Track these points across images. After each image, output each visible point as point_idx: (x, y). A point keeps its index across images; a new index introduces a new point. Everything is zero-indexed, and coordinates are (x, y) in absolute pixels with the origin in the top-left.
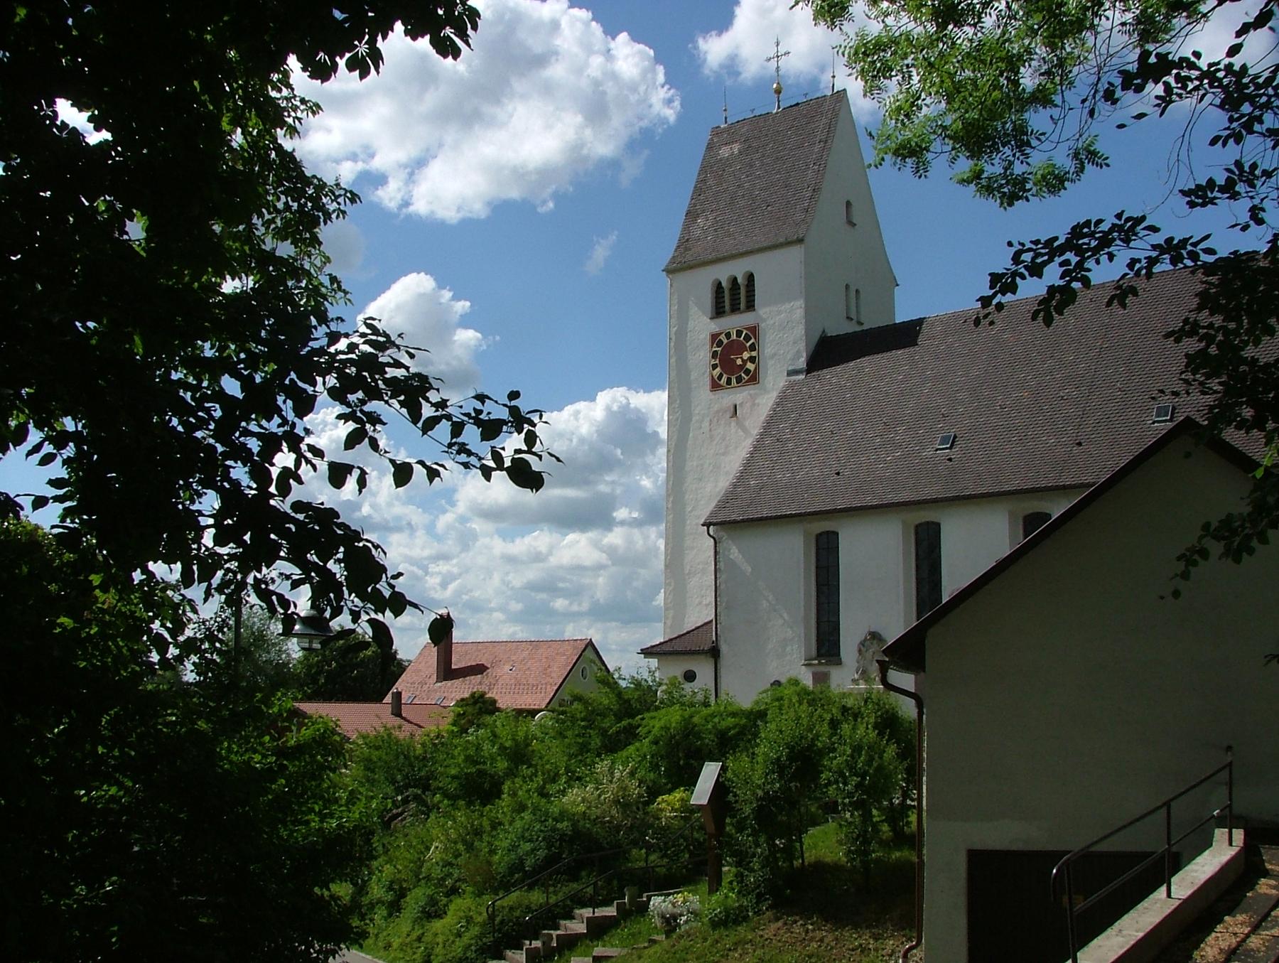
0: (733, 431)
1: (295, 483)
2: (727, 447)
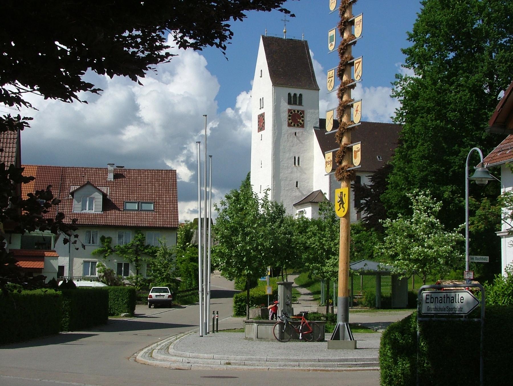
0: (295, 140)
1: (74, 98)
2: (293, 144)
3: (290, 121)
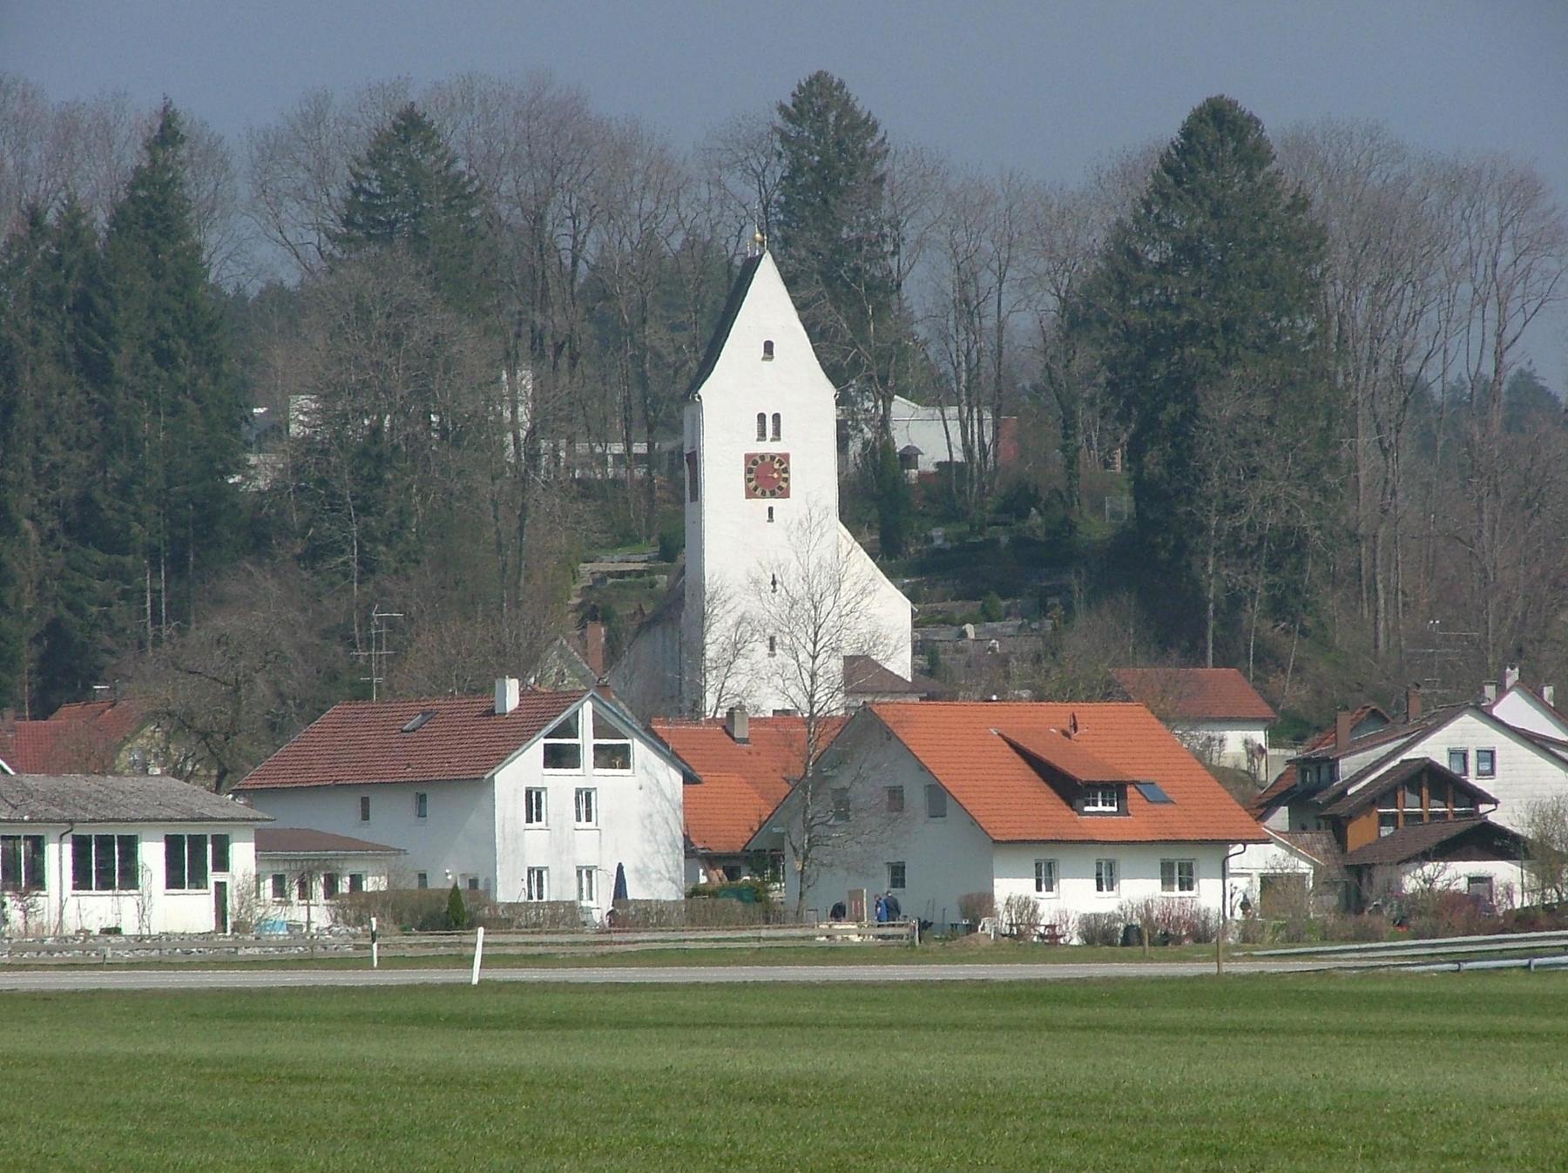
3: (753, 484)
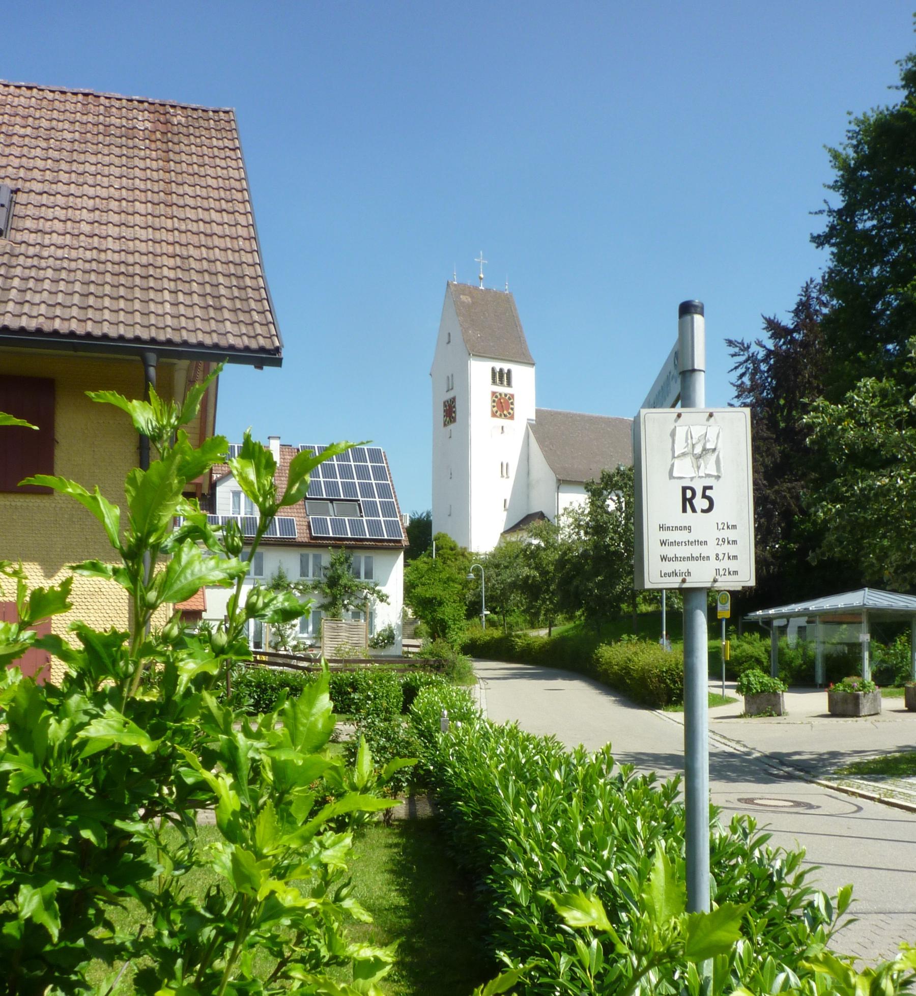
3: (495, 409)
